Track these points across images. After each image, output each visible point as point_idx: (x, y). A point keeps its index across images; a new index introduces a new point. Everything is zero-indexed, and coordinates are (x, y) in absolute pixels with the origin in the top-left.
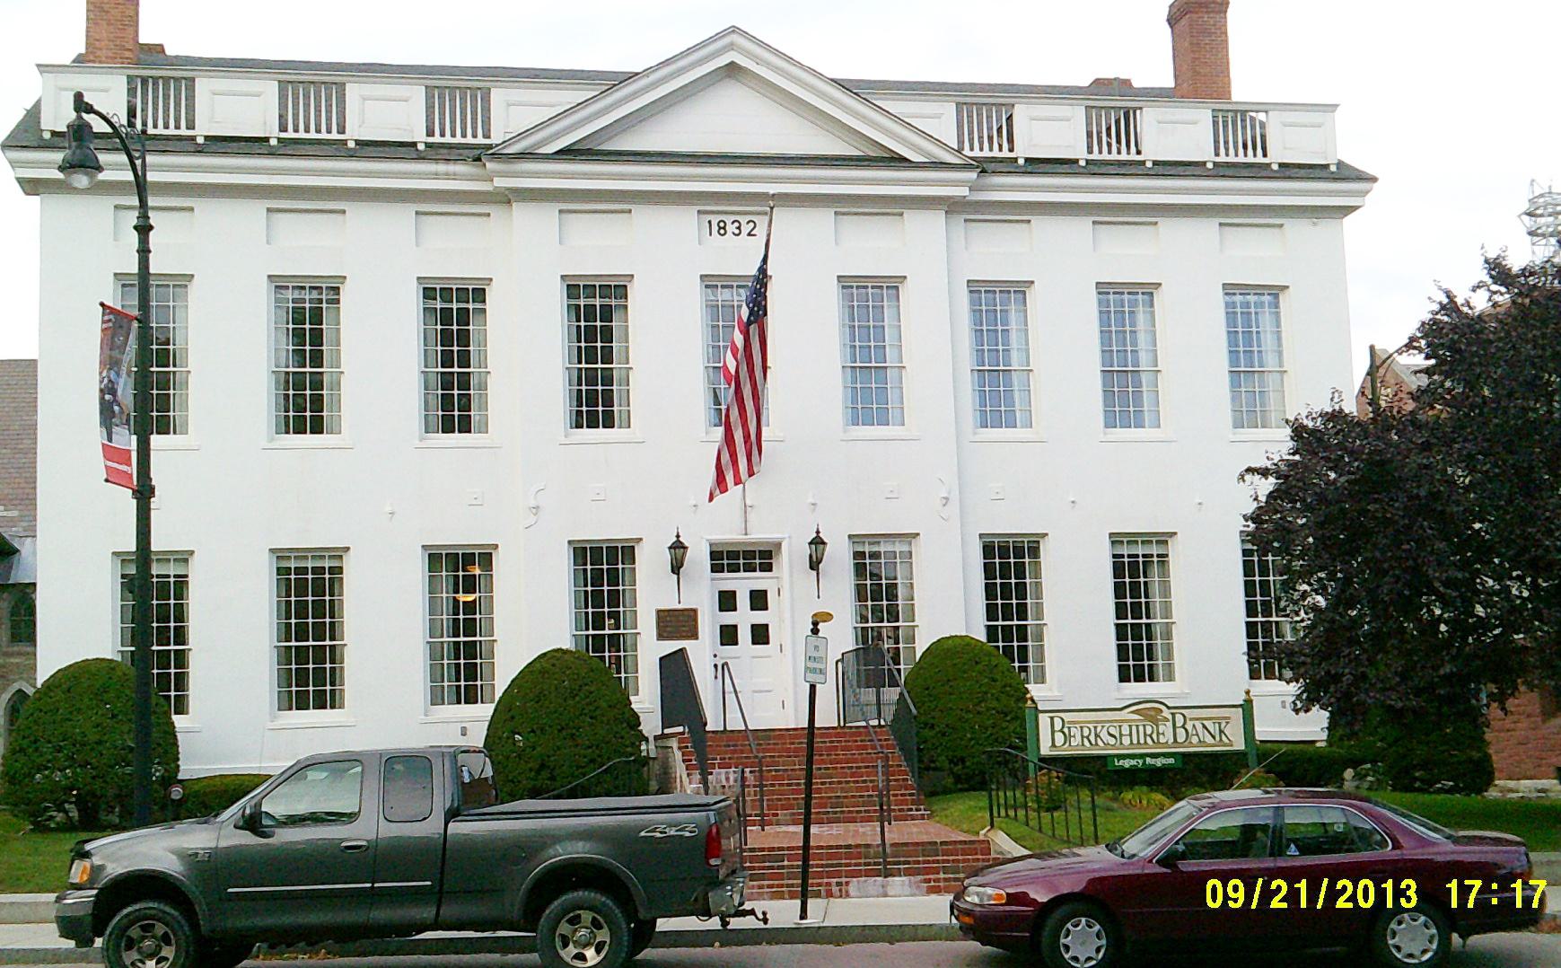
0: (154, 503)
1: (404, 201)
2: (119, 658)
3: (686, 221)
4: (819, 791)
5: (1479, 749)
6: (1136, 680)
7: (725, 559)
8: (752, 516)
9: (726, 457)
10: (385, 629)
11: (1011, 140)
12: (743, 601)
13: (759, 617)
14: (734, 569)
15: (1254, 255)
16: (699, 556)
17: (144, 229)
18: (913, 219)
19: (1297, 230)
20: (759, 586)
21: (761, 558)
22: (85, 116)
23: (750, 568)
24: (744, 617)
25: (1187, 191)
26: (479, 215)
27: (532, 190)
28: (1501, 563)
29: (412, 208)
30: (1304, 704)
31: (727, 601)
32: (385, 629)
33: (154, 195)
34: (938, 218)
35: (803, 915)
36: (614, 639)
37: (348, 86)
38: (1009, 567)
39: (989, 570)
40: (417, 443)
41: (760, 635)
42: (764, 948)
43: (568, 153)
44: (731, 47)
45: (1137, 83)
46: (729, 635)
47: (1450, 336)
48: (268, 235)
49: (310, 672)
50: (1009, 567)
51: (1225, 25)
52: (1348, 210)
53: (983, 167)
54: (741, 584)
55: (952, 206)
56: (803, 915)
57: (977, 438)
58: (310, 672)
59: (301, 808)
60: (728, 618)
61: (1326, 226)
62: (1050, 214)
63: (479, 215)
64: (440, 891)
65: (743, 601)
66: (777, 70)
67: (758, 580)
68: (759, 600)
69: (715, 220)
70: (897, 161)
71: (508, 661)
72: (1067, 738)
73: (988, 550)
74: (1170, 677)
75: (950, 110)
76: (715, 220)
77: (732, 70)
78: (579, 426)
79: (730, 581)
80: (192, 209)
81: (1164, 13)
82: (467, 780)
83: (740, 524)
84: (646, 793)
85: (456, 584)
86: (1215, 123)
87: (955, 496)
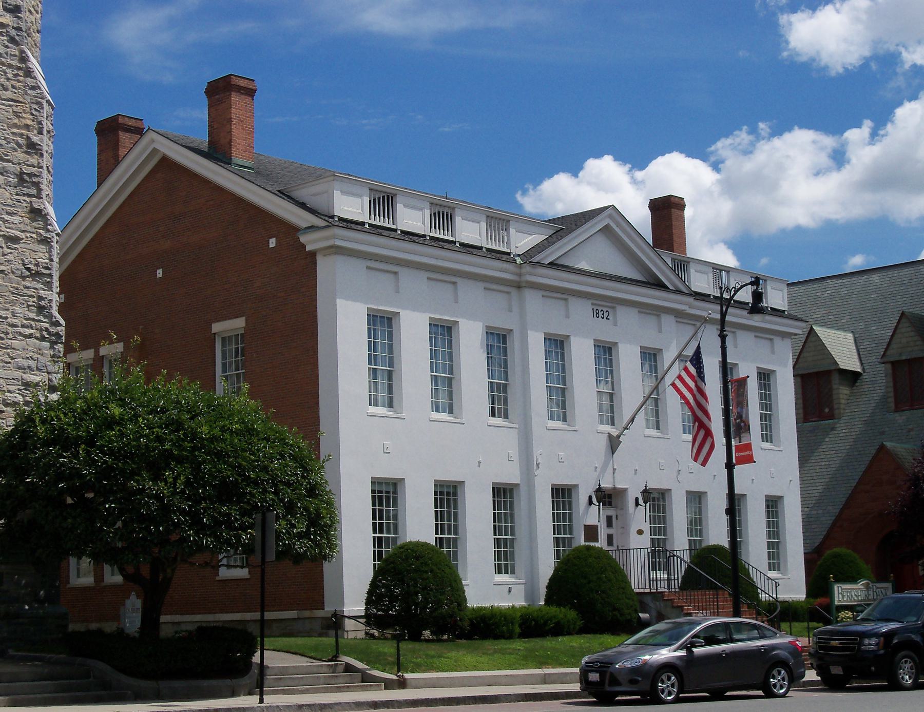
5: (25, 63)
6: (751, 450)
9: (703, 402)
17: (723, 338)
18: (574, 302)
25: (784, 325)
26: (388, 271)
27: (124, 202)
28: (157, 528)
30: (741, 130)
33: (347, 298)
36: (455, 540)
38: (447, 496)
39: (768, 506)
42: (629, 689)
43: (553, 265)
50: (447, 496)
63: (388, 271)
66: (624, 231)
72: (843, 596)
73: (767, 501)
80: (510, 311)
82: (576, 687)
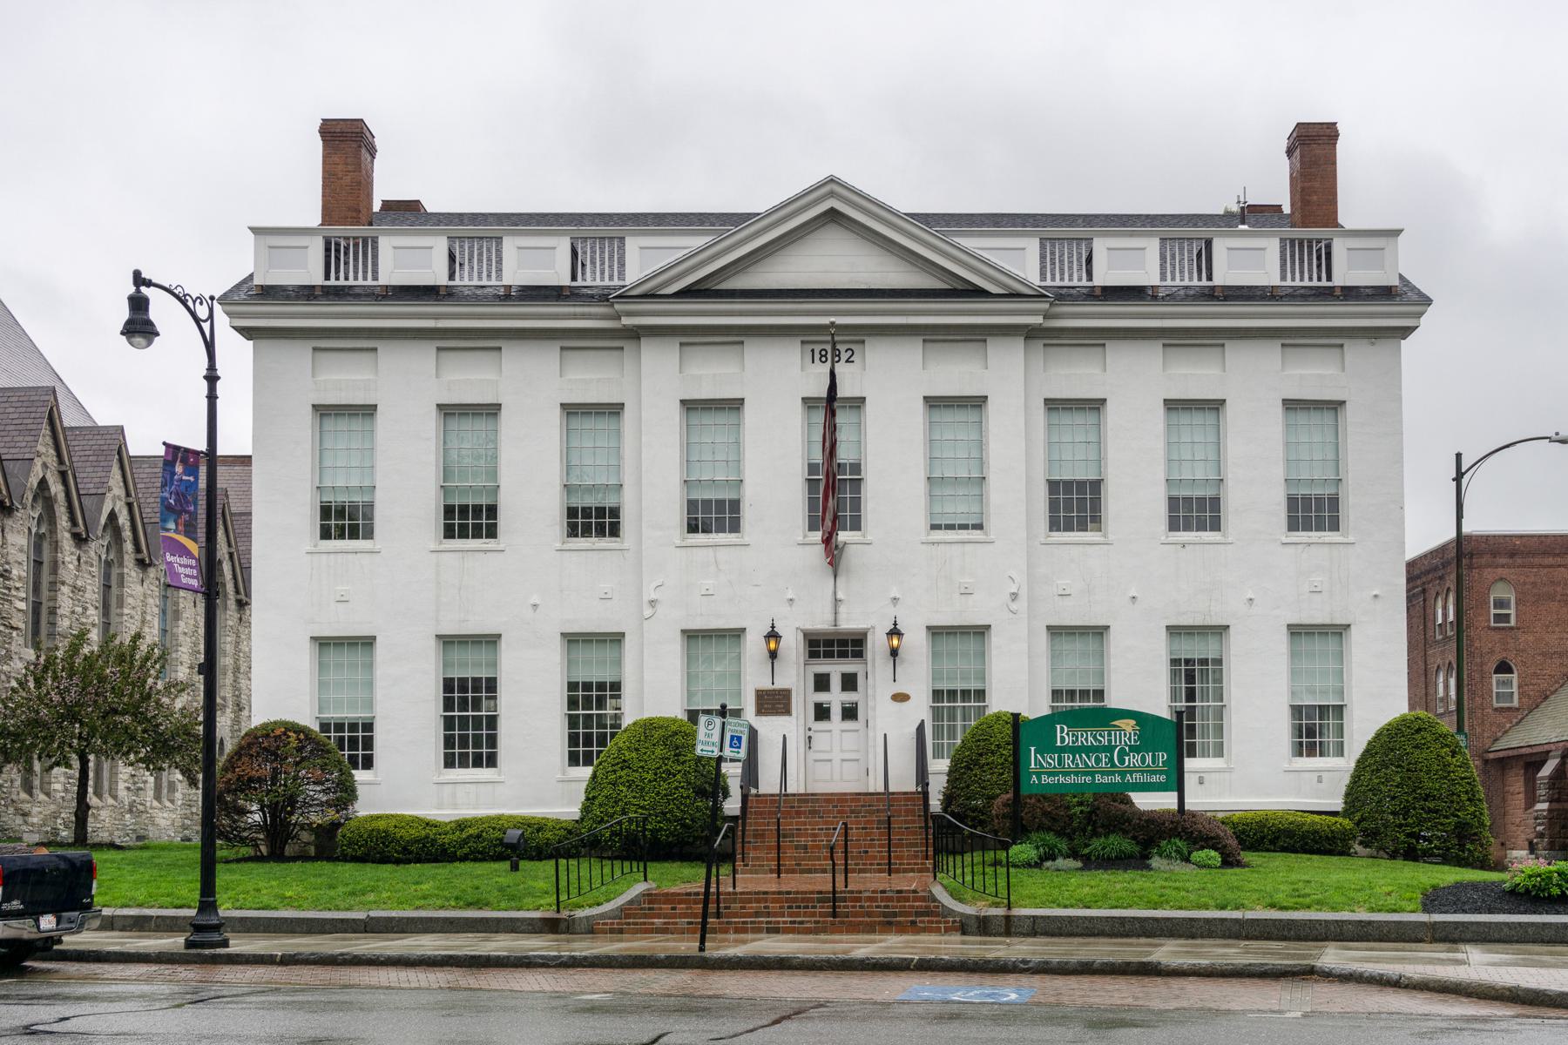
0: (219, 384)
1: (1272, 337)
2: (586, 772)
3: (421, 358)
4: (881, 846)
6: (475, 766)
7: (821, 646)
8: (842, 609)
10: (532, 716)
11: (499, 270)
12: (836, 682)
13: (850, 697)
14: (829, 655)
15: (1313, 375)
16: (792, 645)
19: (1356, 352)
20: (796, 703)
21: (850, 645)
22: (143, 289)
23: (843, 655)
24: (836, 698)
29: (1160, 343)
31: (822, 683)
32: (532, 716)
34: (1018, 344)
35: (702, 949)
37: (505, 239)
40: (558, 545)
41: (850, 713)
44: (832, 194)
45: (431, 207)
46: (822, 713)
47: (1126, 870)
48: (1133, 1024)
49: (469, 730)
51: (1336, 212)
52: (1406, 332)
53: (1063, 296)
54: (835, 669)
55: (1031, 334)
56: (702, 949)
57: (1050, 540)
58: (469, 730)
59: (651, 974)
60: (822, 697)
61: (1382, 348)
62: (769, 339)
64: (831, 413)
65: (836, 682)
67: (849, 667)
68: (849, 682)
69: (817, 348)
70: (978, 293)
71: (1361, 730)
74: (1219, 752)
75: (1032, 246)
76: (817, 348)
77: (833, 216)
78: (1301, 755)
79: (823, 667)
80: (375, 350)
81: (1284, 144)
83: (830, 617)
84: (358, 223)
85: (1300, 731)
86: (328, 250)
87: (1023, 593)
